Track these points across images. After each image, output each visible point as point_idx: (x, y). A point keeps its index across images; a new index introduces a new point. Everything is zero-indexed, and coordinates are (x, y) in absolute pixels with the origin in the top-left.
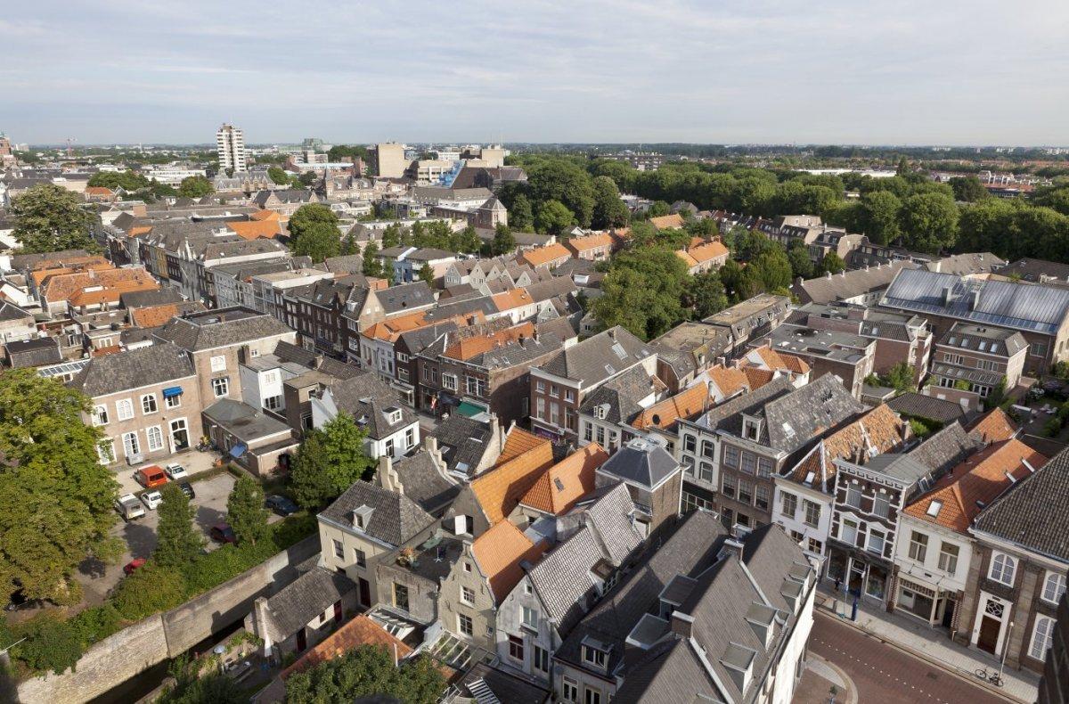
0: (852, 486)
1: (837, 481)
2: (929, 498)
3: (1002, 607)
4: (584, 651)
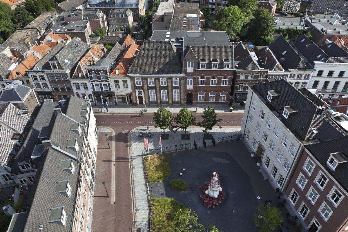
0: (93, 73)
1: (88, 74)
2: (115, 69)
3: (141, 92)
4: (20, 167)
